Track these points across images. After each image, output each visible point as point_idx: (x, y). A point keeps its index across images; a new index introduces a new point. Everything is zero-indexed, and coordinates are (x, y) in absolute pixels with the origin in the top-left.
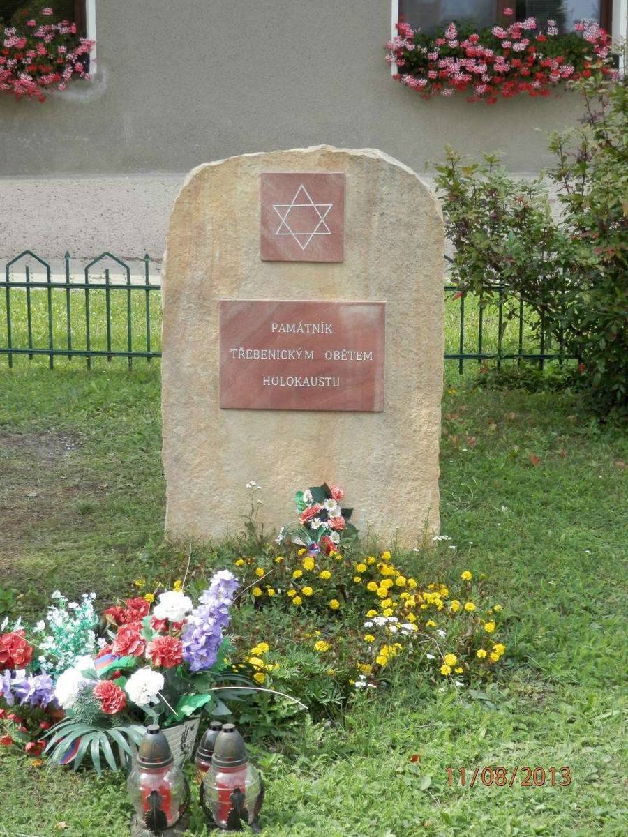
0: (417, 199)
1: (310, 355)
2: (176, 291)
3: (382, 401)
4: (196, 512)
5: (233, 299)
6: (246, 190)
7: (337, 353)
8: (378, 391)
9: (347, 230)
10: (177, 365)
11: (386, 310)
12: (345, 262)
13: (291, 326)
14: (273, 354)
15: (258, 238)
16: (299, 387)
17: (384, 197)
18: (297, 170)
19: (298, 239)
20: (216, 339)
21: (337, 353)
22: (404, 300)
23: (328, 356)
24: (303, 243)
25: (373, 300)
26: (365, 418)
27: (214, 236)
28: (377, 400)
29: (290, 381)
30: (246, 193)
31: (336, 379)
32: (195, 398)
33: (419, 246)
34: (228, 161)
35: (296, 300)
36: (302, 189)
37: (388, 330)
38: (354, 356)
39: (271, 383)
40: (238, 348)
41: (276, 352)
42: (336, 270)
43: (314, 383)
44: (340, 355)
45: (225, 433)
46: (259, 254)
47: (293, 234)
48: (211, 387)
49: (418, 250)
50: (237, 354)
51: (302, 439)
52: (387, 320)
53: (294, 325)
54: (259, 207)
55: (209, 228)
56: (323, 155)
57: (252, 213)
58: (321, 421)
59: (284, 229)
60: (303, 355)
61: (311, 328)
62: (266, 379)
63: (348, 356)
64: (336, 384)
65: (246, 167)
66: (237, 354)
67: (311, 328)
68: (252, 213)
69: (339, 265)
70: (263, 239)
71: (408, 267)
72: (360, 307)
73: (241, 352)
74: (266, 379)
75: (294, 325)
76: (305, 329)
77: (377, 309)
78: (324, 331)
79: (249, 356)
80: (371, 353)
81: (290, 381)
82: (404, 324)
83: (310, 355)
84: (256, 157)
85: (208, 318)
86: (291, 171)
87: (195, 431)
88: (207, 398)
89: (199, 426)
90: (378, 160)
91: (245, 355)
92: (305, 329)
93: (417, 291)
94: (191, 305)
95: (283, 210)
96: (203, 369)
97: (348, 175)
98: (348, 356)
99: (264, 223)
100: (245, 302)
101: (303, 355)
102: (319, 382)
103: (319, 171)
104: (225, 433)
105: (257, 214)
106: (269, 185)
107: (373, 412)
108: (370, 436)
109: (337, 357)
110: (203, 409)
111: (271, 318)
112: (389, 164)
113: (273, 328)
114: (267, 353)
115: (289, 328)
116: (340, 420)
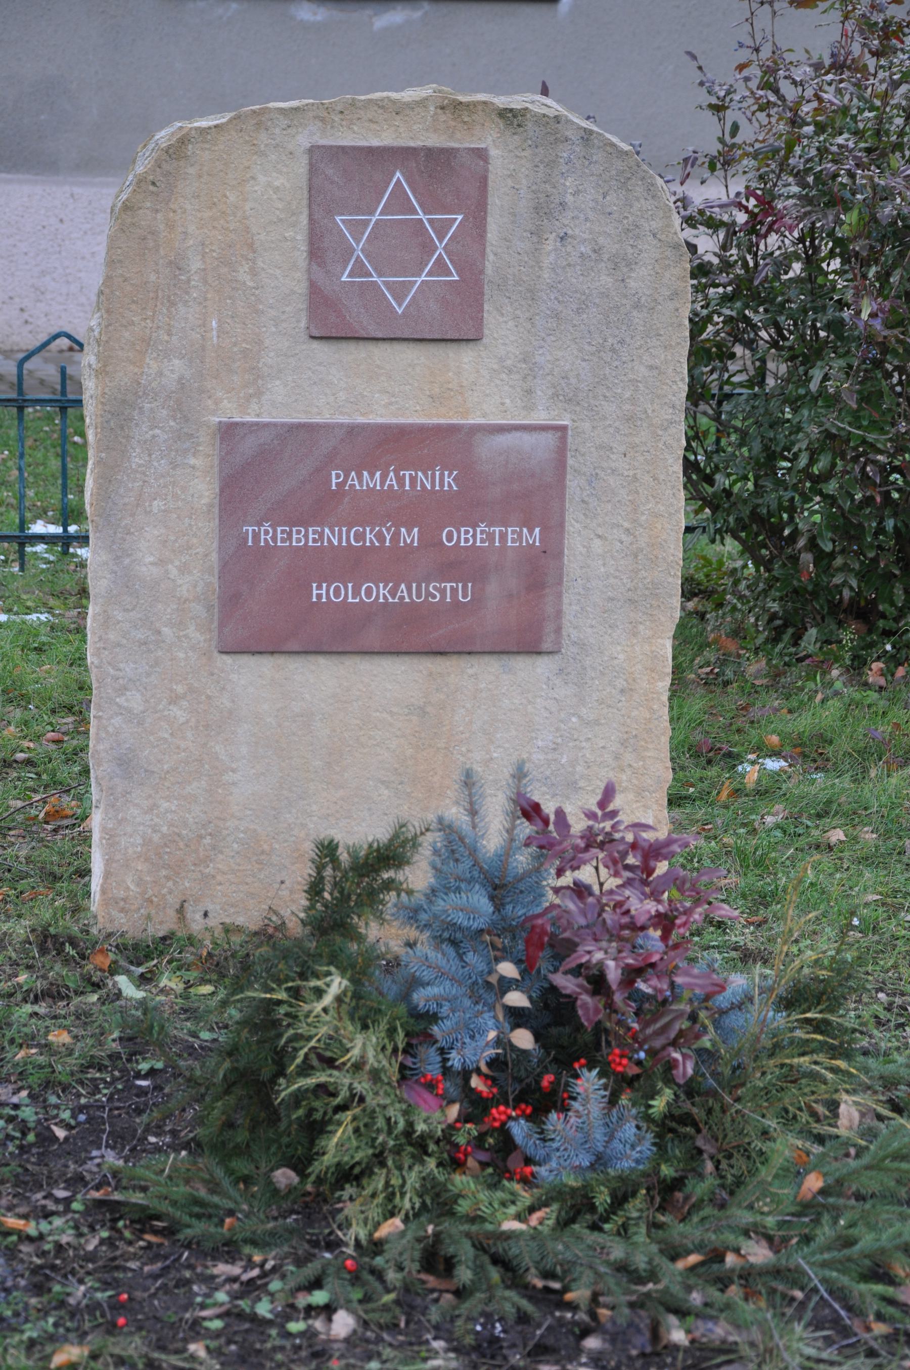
0: (637, 205)
1: (411, 537)
2: (124, 401)
3: (558, 630)
4: (164, 872)
5: (248, 419)
6: (277, 183)
7: (467, 532)
8: (550, 610)
9: (489, 269)
10: (127, 561)
11: (570, 439)
12: (484, 340)
13: (372, 475)
14: (333, 536)
15: (302, 288)
16: (386, 604)
17: (569, 199)
18: (384, 138)
19: (388, 289)
20: (211, 505)
21: (467, 532)
22: (605, 418)
23: (450, 539)
24: (399, 300)
25: (540, 417)
26: (521, 664)
27: (205, 282)
28: (549, 627)
29: (369, 592)
30: (277, 190)
31: (465, 588)
32: (166, 630)
33: (637, 306)
34: (237, 117)
35: (380, 420)
36: (398, 179)
37: (573, 484)
38: (503, 536)
39: (378, 588)
40: (259, 524)
41: (340, 532)
42: (466, 356)
43: (419, 597)
44: (474, 536)
45: (228, 704)
46: (303, 324)
47: (419, 280)
48: (198, 609)
49: (635, 313)
50: (256, 536)
51: (391, 713)
52: (570, 462)
53: (378, 474)
54: (304, 220)
55: (196, 265)
56: (442, 108)
57: (289, 234)
58: (431, 674)
59: (359, 270)
60: (396, 537)
61: (413, 480)
62: (319, 587)
63: (491, 537)
64: (464, 597)
65: (277, 131)
66: (256, 536)
67: (413, 480)
68: (289, 234)
69: (471, 345)
70: (314, 290)
71: (613, 350)
72: (518, 434)
73: (266, 532)
74: (319, 587)
75: (378, 474)
76: (400, 480)
77: (549, 439)
78: (442, 484)
79: (283, 540)
80: (537, 530)
81: (369, 592)
82: (603, 469)
83: (411, 537)
84: (296, 109)
85: (192, 461)
86: (375, 143)
87: (164, 702)
88: (192, 631)
89: (171, 690)
90: (557, 119)
91: (274, 538)
92: (400, 480)
93: (633, 400)
94: (157, 431)
95: (357, 228)
96: (184, 569)
97: (494, 152)
98: (491, 537)
99: (315, 253)
100: (275, 425)
101: (396, 537)
102: (428, 594)
103: (433, 141)
104: (228, 704)
105: (300, 236)
106: (330, 172)
107: (539, 653)
108: (530, 702)
109: (467, 540)
110: (181, 655)
111: (330, 461)
112: (580, 128)
113: (334, 481)
114: (321, 535)
115: (371, 481)
116: (470, 671)
